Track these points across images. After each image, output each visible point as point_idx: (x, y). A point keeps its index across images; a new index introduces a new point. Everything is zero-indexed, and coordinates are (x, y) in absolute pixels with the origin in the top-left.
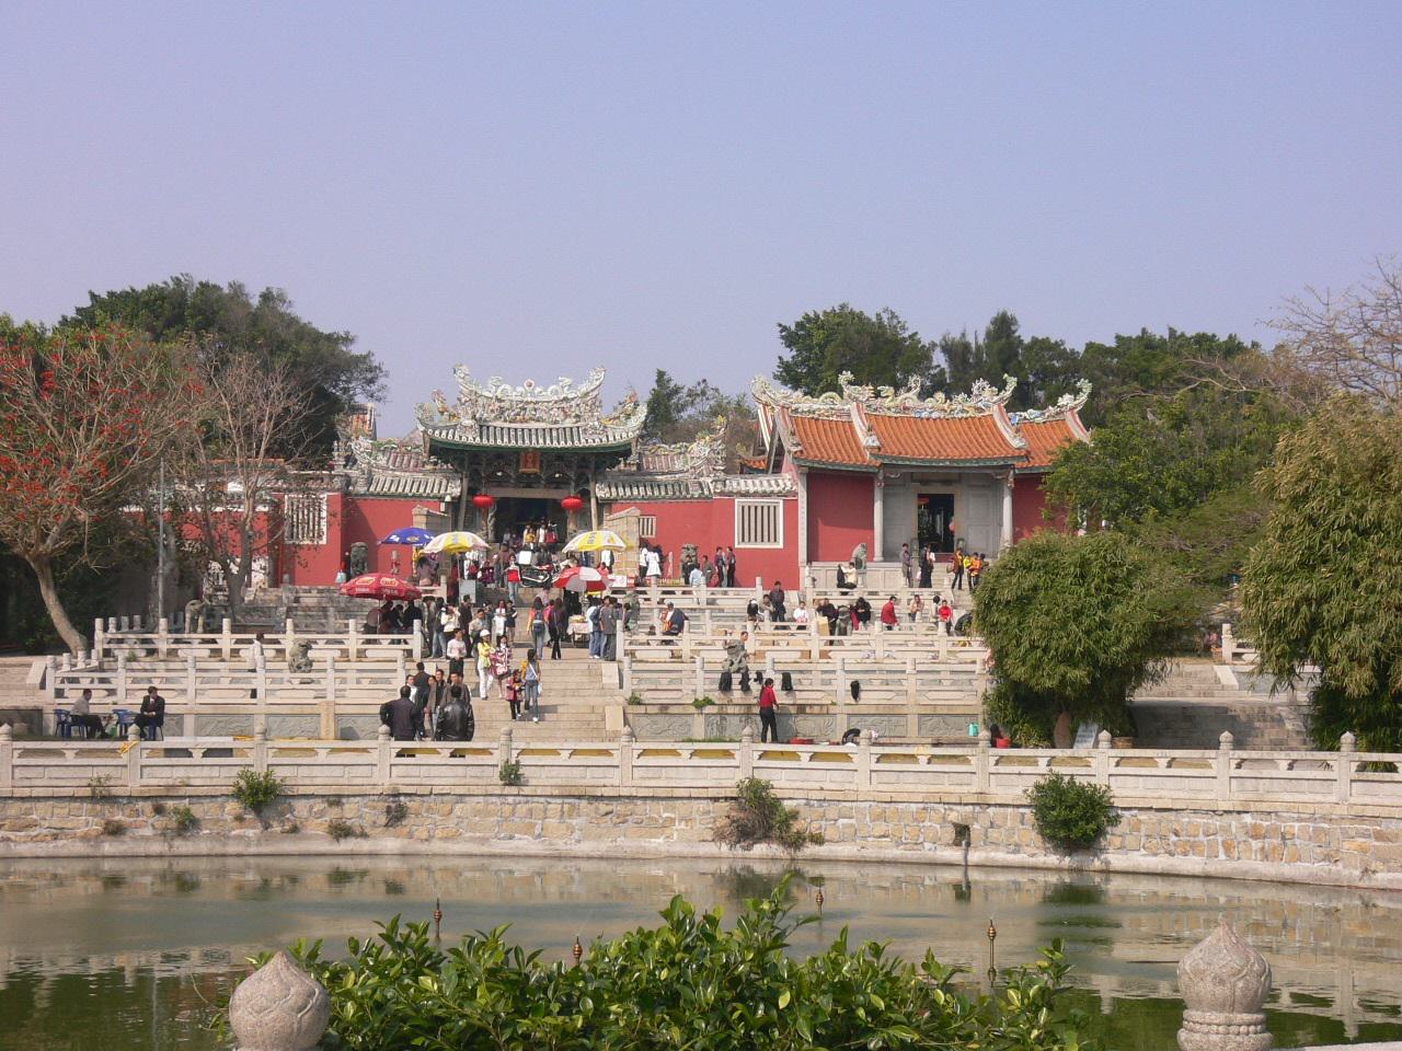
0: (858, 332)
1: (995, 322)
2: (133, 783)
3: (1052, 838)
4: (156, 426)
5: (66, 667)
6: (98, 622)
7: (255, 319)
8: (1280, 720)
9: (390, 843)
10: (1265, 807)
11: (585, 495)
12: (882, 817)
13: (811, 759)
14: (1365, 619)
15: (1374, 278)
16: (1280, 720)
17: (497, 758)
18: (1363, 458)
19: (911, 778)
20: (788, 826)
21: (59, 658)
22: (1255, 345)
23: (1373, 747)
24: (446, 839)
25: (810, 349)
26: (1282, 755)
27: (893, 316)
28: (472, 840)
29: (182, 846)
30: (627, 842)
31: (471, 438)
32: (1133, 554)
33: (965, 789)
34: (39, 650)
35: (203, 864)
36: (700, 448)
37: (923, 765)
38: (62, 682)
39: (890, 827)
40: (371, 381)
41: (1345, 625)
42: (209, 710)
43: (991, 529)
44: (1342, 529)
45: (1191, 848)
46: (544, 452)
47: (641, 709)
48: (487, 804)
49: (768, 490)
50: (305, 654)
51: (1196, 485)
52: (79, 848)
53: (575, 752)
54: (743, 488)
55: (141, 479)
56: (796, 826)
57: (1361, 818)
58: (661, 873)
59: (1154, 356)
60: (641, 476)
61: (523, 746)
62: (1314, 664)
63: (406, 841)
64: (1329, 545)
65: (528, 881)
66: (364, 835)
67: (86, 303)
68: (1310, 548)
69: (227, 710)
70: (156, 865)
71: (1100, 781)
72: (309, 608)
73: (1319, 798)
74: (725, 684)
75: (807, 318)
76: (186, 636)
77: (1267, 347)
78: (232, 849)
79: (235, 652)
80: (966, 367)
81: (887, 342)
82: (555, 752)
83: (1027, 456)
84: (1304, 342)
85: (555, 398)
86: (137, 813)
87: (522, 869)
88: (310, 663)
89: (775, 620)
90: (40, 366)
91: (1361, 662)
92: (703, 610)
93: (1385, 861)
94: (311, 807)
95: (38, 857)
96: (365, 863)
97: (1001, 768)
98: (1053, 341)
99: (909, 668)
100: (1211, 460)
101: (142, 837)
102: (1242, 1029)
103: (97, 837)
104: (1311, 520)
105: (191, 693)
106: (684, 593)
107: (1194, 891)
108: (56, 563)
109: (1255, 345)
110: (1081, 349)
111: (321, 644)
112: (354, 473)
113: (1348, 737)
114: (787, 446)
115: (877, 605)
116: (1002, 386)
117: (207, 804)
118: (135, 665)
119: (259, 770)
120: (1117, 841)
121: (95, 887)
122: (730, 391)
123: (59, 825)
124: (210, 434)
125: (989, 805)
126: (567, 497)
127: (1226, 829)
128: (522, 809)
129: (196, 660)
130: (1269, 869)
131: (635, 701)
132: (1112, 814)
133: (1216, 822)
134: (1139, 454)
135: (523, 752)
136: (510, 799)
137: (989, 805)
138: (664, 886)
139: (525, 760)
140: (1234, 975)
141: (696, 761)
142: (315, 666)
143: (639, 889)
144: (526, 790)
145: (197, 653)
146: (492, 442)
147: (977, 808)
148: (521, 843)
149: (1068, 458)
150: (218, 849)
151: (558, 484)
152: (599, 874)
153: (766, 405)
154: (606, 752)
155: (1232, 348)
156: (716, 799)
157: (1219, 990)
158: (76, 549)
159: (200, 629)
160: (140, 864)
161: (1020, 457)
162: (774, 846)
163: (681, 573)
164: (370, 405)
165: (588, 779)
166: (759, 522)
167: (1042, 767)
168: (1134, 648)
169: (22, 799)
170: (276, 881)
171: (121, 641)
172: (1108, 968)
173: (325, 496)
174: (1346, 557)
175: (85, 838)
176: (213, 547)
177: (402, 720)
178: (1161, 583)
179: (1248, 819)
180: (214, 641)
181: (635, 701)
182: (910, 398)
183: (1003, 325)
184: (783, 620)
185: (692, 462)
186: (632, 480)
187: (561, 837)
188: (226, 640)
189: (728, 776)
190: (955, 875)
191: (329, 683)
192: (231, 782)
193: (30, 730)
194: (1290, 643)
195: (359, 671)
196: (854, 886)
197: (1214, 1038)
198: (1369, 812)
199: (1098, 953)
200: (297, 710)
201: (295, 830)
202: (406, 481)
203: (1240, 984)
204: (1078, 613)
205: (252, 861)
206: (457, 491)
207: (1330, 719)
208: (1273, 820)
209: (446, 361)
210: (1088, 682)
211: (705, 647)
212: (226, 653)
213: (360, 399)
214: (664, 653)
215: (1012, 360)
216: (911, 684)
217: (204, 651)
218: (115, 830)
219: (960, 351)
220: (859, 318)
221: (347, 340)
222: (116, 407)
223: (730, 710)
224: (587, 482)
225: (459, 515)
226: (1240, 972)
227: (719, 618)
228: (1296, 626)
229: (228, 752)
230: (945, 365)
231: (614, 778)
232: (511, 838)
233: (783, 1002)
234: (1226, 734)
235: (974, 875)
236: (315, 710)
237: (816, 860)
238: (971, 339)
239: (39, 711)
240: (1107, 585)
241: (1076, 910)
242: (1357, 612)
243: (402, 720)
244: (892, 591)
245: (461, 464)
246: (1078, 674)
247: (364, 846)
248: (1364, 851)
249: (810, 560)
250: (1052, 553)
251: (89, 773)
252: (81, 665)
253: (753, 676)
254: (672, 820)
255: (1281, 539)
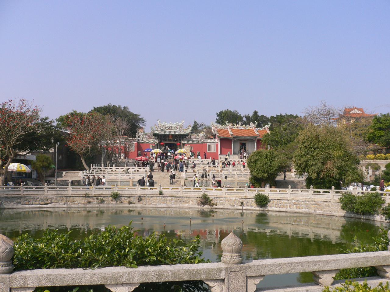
0: (230, 114)
1: (254, 112)
2: (93, 194)
3: (258, 205)
4: (102, 130)
5: (85, 173)
6: (91, 165)
7: (123, 112)
8: (302, 183)
9: (139, 205)
10: (296, 199)
11: (180, 143)
12: (227, 201)
13: (215, 190)
14: (315, 165)
15: (321, 104)
16: (302, 183)
17: (158, 190)
18: (315, 135)
19: (233, 194)
20: (211, 202)
21: (83, 171)
22: (300, 116)
23: (317, 188)
24: (149, 204)
25: (222, 117)
26: (300, 189)
27: (236, 111)
28: (154, 204)
29: (101, 205)
30: (181, 205)
31: (160, 133)
32: (276, 153)
33: (243, 196)
34: (80, 170)
35: (105, 209)
36: (201, 134)
37: (235, 191)
38: (84, 175)
39: (229, 202)
40: (143, 122)
41: (312, 166)
42: (110, 181)
43: (253, 148)
44: (311, 148)
45: (283, 207)
46: (173, 135)
47: (187, 181)
48: (156, 198)
49: (213, 142)
50: (128, 171)
51: (288, 141)
52: (83, 206)
53: (172, 189)
54: (208, 142)
55: (100, 140)
56: (212, 202)
57: (314, 201)
58: (188, 210)
59: (283, 118)
60: (191, 139)
61: (163, 187)
62: (306, 173)
63: (142, 205)
64: (309, 151)
65: (164, 212)
66: (134, 203)
67: (93, 109)
68: (305, 152)
69: (113, 181)
70: (97, 209)
71: (267, 194)
72: (130, 163)
73: (306, 197)
74: (203, 176)
75: (221, 112)
76: (107, 167)
77: (303, 117)
78: (110, 206)
79: (115, 170)
80: (249, 120)
81: (235, 116)
82: (169, 189)
83: (259, 136)
84: (308, 116)
85: (175, 125)
86: (94, 199)
87: (163, 210)
88: (129, 172)
89: (213, 165)
90: (81, 119)
91: (315, 173)
92: (200, 163)
93: (318, 209)
94: (125, 198)
95: (75, 207)
96: (134, 209)
97: (249, 192)
98: (265, 116)
99: (236, 174)
100: (291, 136)
101: (94, 204)
102: (234, 257)
103: (86, 204)
104: (306, 147)
105: (119, 178)
106: (197, 160)
107: (284, 214)
108: (84, 154)
109: (300, 116)
110: (270, 117)
111: (131, 169)
112: (139, 139)
113: (312, 186)
114: (216, 134)
115: (232, 162)
116: (255, 123)
117: (106, 198)
118: (98, 173)
119: (115, 192)
120: (270, 205)
121: (86, 213)
122: (207, 124)
123: (79, 201)
124: (114, 132)
125: (247, 199)
126: (177, 143)
127: (290, 203)
128: (163, 199)
129: (108, 172)
130: (297, 210)
131: (186, 179)
132: (269, 200)
133: (288, 202)
134: (278, 135)
135: (163, 189)
136: (161, 197)
137: (247, 199)
138: (188, 213)
139: (163, 190)
140: (232, 245)
141: (194, 190)
142: (129, 173)
143: (184, 213)
144: (163, 196)
145: (109, 171)
146: (164, 133)
147: (245, 199)
148: (162, 205)
149: (265, 136)
150: (108, 206)
151: (176, 141)
152: (176, 211)
153: (213, 127)
154: (178, 189)
155: (297, 117)
156: (198, 197)
157: (229, 248)
158: (88, 152)
159: (110, 166)
160: (94, 208)
161: (258, 136)
162: (208, 206)
163: (197, 157)
164: (143, 127)
165: (175, 194)
166: (211, 148)
167: (257, 192)
168: (276, 170)
169: (73, 197)
170: (118, 212)
171: (96, 168)
172: (269, 227)
173: (134, 143)
174: (312, 153)
175: (84, 204)
176: (113, 152)
177: (142, 183)
178: (281, 159)
179: (293, 201)
180: (112, 168)
181: (186, 179)
182: (239, 126)
183: (256, 113)
184: (215, 165)
185: (200, 137)
186: (188, 140)
187: (170, 204)
188: (114, 168)
189: (200, 193)
190: (241, 211)
191: (131, 176)
192: (110, 194)
193: (78, 184)
194: (302, 169)
195: (138, 174)
196: (222, 213)
197: (228, 259)
198: (315, 200)
199: (267, 225)
200: (126, 181)
201: (122, 202)
202: (149, 140)
203: (234, 247)
204: (266, 164)
205: (114, 208)
206: (158, 142)
207: (310, 183)
208: (298, 201)
209: (157, 119)
210: (267, 176)
211: (199, 171)
212: (114, 171)
213: (141, 126)
214: (192, 171)
215: (258, 119)
216: (236, 176)
217: (110, 170)
218: (89, 202)
219: (248, 117)
220: (230, 112)
221: (139, 115)
222: (95, 127)
223: (203, 181)
224: (181, 140)
225: (158, 146)
226: (234, 244)
227: (203, 165)
228: (303, 166)
229: (110, 188)
230: (245, 120)
231: (179, 193)
232: (161, 204)
233: (127, 250)
234: (290, 186)
235: (244, 211)
236: (129, 181)
237: (216, 208)
238: (250, 115)
239: (80, 181)
240: (271, 159)
241: (262, 218)
242: (314, 164)
243: (142, 183)
244: (234, 160)
245: (158, 138)
246: (266, 175)
247: (134, 205)
248: (314, 207)
249: (221, 154)
250: (261, 153)
251: (85, 192)
252: (88, 173)
253: (207, 175)
254: (190, 201)
255: (300, 150)
